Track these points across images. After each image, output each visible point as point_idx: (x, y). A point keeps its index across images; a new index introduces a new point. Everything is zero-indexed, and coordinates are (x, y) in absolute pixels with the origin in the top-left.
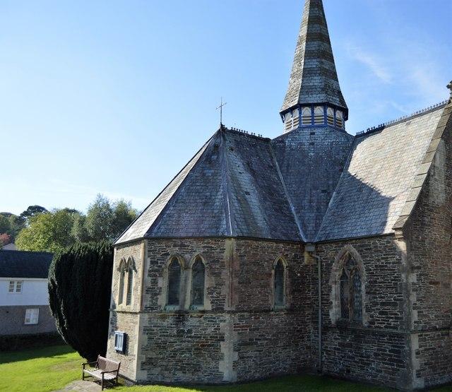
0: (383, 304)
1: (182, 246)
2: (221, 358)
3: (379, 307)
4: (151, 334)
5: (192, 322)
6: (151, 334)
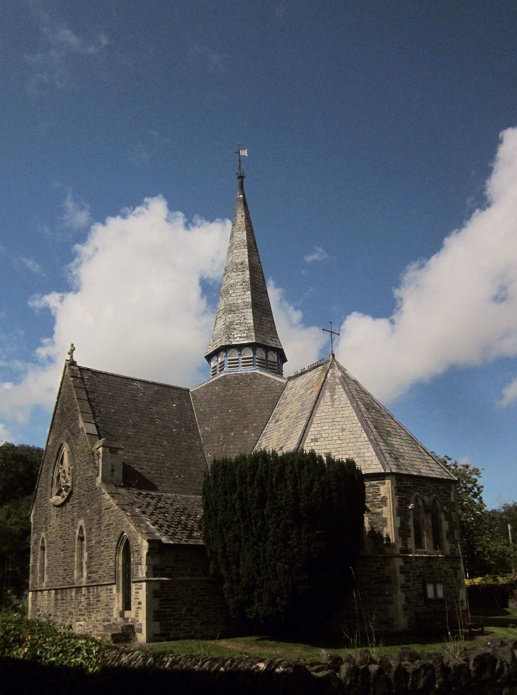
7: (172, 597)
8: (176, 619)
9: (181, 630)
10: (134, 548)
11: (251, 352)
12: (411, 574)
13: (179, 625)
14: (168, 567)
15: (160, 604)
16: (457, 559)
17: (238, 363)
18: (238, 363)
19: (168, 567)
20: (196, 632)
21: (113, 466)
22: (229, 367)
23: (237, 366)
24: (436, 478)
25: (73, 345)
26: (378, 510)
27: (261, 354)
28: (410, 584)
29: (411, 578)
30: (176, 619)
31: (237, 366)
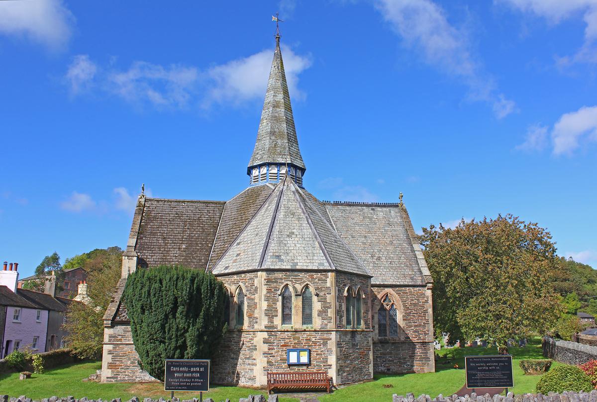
0: (416, 326)
1: (351, 280)
2: (368, 364)
3: (413, 328)
4: (341, 347)
5: (358, 337)
6: (341, 347)
7: (121, 354)
8: (123, 368)
9: (126, 375)
10: (130, 329)
11: (276, 169)
12: (275, 344)
13: (125, 372)
14: (120, 335)
15: (112, 359)
16: (73, 267)
17: (258, 178)
18: (258, 178)
19: (120, 335)
20: (137, 377)
21: (129, 268)
22: (254, 182)
23: (258, 181)
24: (273, 269)
25: (441, 224)
26: (253, 297)
27: (293, 172)
28: (273, 351)
29: (275, 347)
30: (123, 368)
31: (258, 181)
